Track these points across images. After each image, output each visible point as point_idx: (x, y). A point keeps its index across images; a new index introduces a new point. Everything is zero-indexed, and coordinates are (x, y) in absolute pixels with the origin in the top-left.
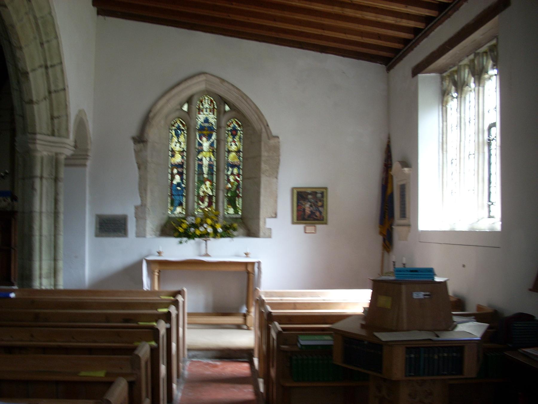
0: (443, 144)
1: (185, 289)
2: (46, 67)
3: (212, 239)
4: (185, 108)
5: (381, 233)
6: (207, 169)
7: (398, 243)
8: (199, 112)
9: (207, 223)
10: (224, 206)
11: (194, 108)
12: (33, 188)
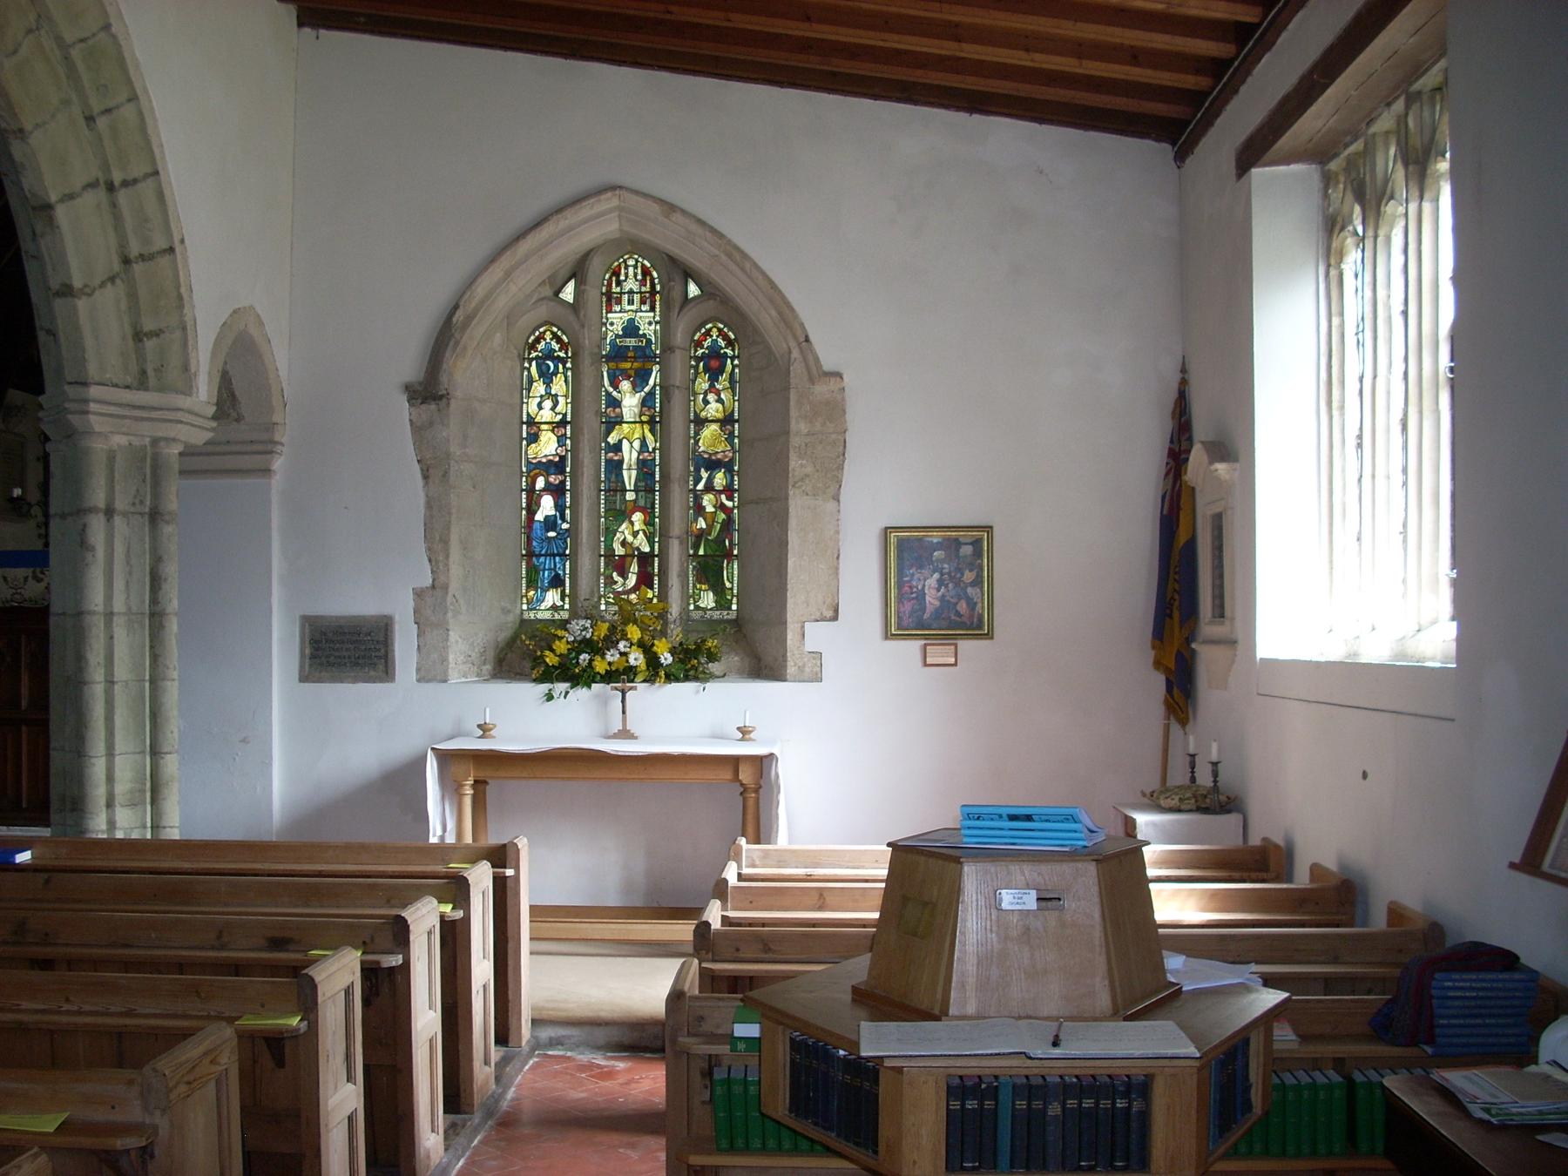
0: (1330, 383)
1: (522, 843)
2: (111, 188)
3: (642, 687)
4: (568, 294)
5: (1158, 664)
7: (1209, 696)
9: (552, 651)
10: (685, 585)
11: (593, 294)
12: (83, 544)
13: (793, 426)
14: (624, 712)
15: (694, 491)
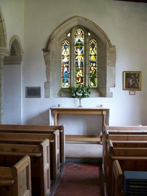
1: (64, 126)
4: (69, 35)
6: (80, 64)
8: (76, 36)
11: (73, 35)
13: (107, 55)
14: (80, 103)
15: (90, 67)
